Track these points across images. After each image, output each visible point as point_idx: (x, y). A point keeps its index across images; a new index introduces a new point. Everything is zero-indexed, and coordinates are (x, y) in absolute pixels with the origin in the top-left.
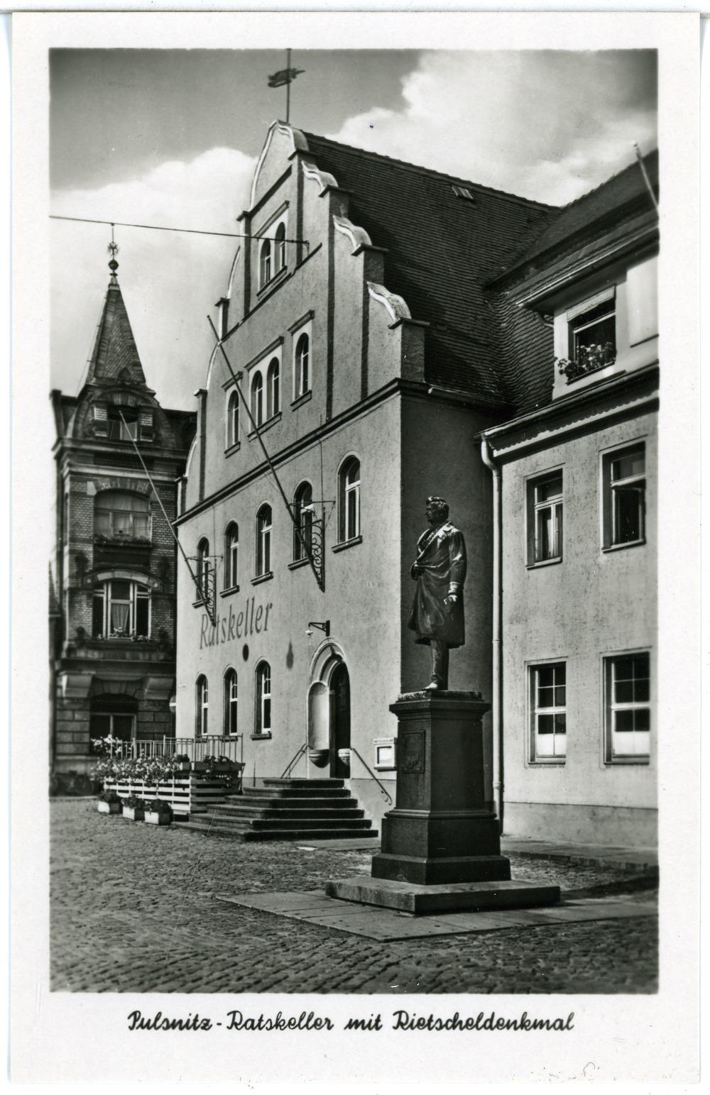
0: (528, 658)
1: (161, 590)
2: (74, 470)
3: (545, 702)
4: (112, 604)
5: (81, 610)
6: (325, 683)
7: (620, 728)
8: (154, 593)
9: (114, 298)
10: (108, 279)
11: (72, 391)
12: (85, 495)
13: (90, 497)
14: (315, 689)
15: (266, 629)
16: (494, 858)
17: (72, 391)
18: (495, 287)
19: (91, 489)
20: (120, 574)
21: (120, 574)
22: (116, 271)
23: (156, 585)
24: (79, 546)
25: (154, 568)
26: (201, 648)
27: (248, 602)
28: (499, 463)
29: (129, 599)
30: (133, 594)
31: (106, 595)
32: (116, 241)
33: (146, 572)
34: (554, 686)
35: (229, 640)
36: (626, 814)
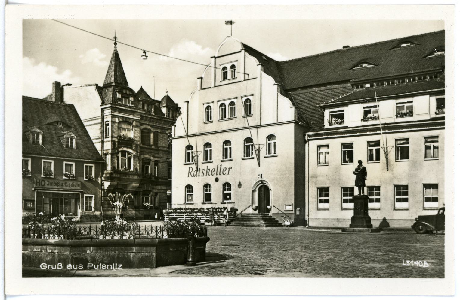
0: (317, 186)
1: (136, 154)
2: (112, 114)
3: (320, 197)
4: (122, 159)
5: (114, 160)
6: (257, 189)
7: (426, 201)
8: (134, 156)
9: (116, 57)
10: (113, 49)
11: (101, 85)
12: (115, 122)
13: (117, 123)
14: (254, 191)
15: (228, 174)
16: (38, 269)
17: (101, 85)
18: (324, 108)
19: (117, 120)
20: (125, 149)
21: (125, 149)
22: (116, 46)
23: (134, 153)
24: (114, 139)
25: (133, 148)
26: (188, 177)
27: (218, 166)
28: (309, 140)
29: (126, 157)
30: (127, 155)
31: (120, 155)
32: (117, 36)
33: (132, 149)
34: (348, 192)
36: (342, 220)
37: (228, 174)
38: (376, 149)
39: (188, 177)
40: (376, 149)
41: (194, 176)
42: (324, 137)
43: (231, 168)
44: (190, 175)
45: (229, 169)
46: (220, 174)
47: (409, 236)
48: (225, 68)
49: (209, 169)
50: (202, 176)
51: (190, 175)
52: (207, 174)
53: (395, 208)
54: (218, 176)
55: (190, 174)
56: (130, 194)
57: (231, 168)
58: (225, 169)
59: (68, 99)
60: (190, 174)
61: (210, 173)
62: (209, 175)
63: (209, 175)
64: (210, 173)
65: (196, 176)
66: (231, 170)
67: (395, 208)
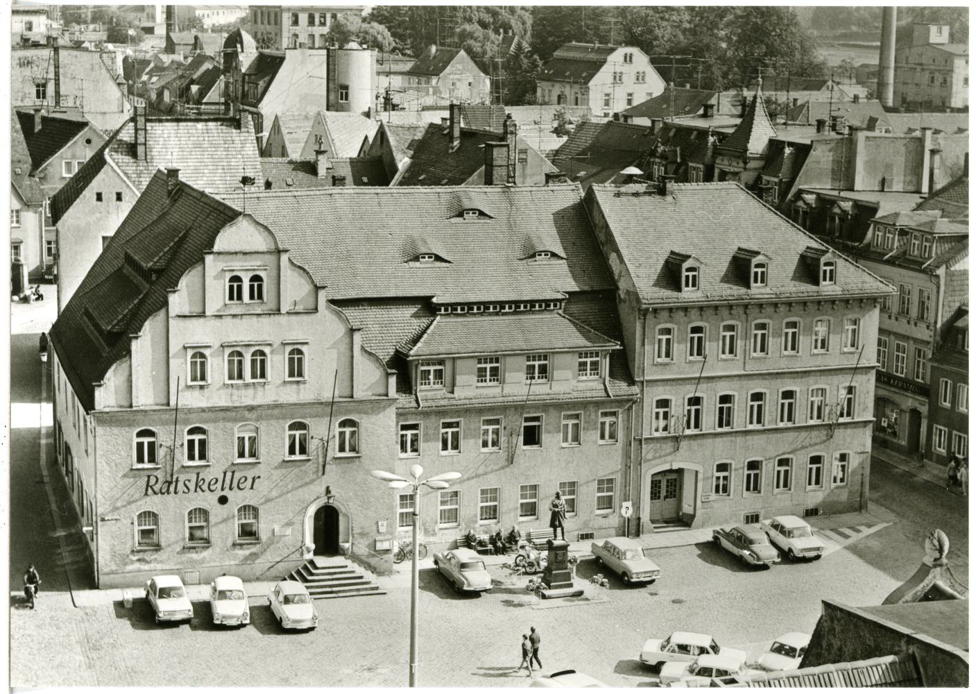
15: (252, 488)
24: (246, 130)
26: (146, 494)
35: (196, 491)
37: (252, 488)
38: (149, 443)
39: (146, 494)
40: (149, 443)
41: (163, 494)
42: (361, 593)
43: (259, 477)
44: (150, 491)
45: (254, 479)
46: (231, 489)
47: (270, 518)
48: (626, 54)
49: (203, 480)
50: (184, 492)
51: (150, 491)
52: (198, 489)
53: (857, 129)
54: (226, 493)
55: (149, 489)
56: (563, 413)
57: (259, 477)
58: (244, 479)
59: (272, 607)
60: (149, 489)
61: (205, 487)
62: (203, 491)
63: (203, 491)
64: (205, 487)
65: (168, 493)
66: (257, 481)
67: (857, 129)
